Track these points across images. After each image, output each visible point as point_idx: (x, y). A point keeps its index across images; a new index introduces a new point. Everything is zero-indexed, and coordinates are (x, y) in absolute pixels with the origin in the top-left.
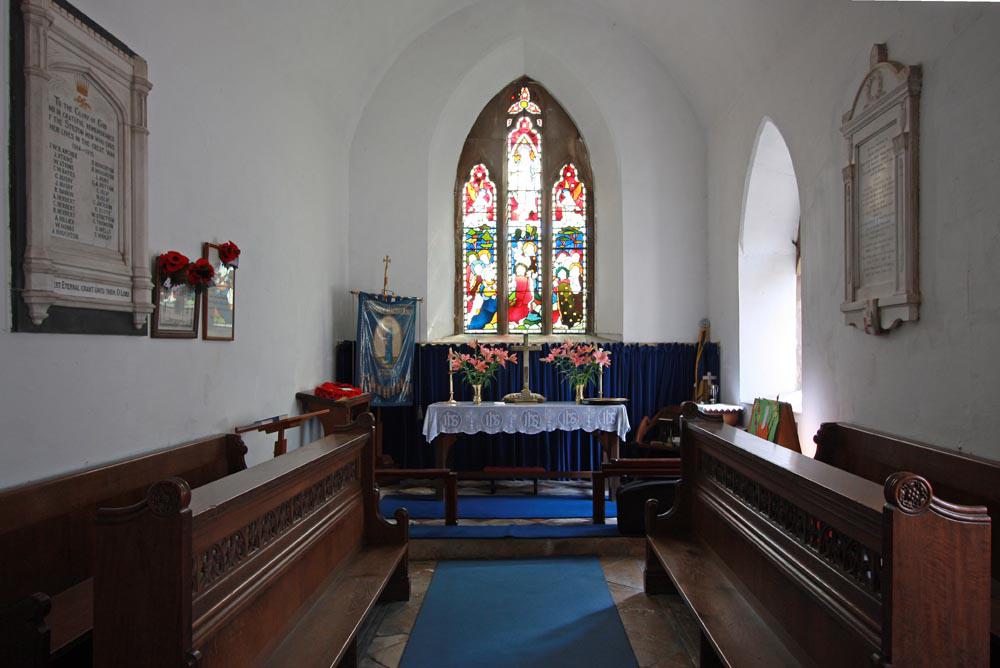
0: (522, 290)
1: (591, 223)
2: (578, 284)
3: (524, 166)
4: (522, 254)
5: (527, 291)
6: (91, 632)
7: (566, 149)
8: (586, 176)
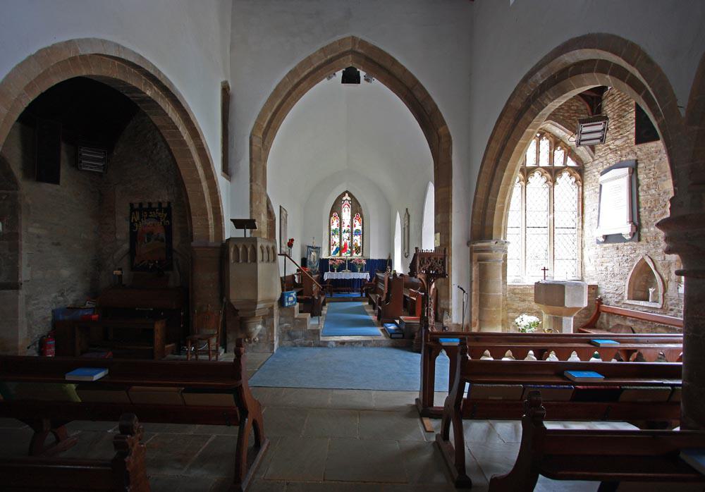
0: (346, 245)
1: (363, 228)
3: (346, 215)
7: (356, 210)
8: (362, 216)
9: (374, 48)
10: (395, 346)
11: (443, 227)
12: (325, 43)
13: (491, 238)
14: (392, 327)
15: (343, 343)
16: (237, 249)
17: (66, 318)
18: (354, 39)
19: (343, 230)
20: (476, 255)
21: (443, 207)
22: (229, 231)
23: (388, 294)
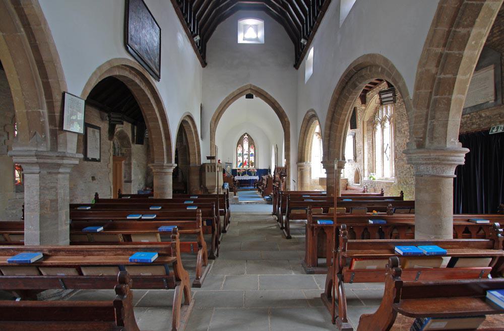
0: (246, 162)
1: (255, 153)
2: (219, 254)
3: (246, 145)
4: (245, 157)
5: (429, 140)
6: (132, 241)
7: (251, 143)
8: (254, 146)
9: (259, 88)
10: (268, 204)
11: (287, 157)
12: (240, 87)
13: (304, 161)
14: (268, 197)
15: (248, 203)
16: (208, 167)
17: (143, 193)
18: (251, 85)
19: (244, 154)
20: (299, 168)
21: (287, 149)
22: (204, 160)
23: (266, 185)
